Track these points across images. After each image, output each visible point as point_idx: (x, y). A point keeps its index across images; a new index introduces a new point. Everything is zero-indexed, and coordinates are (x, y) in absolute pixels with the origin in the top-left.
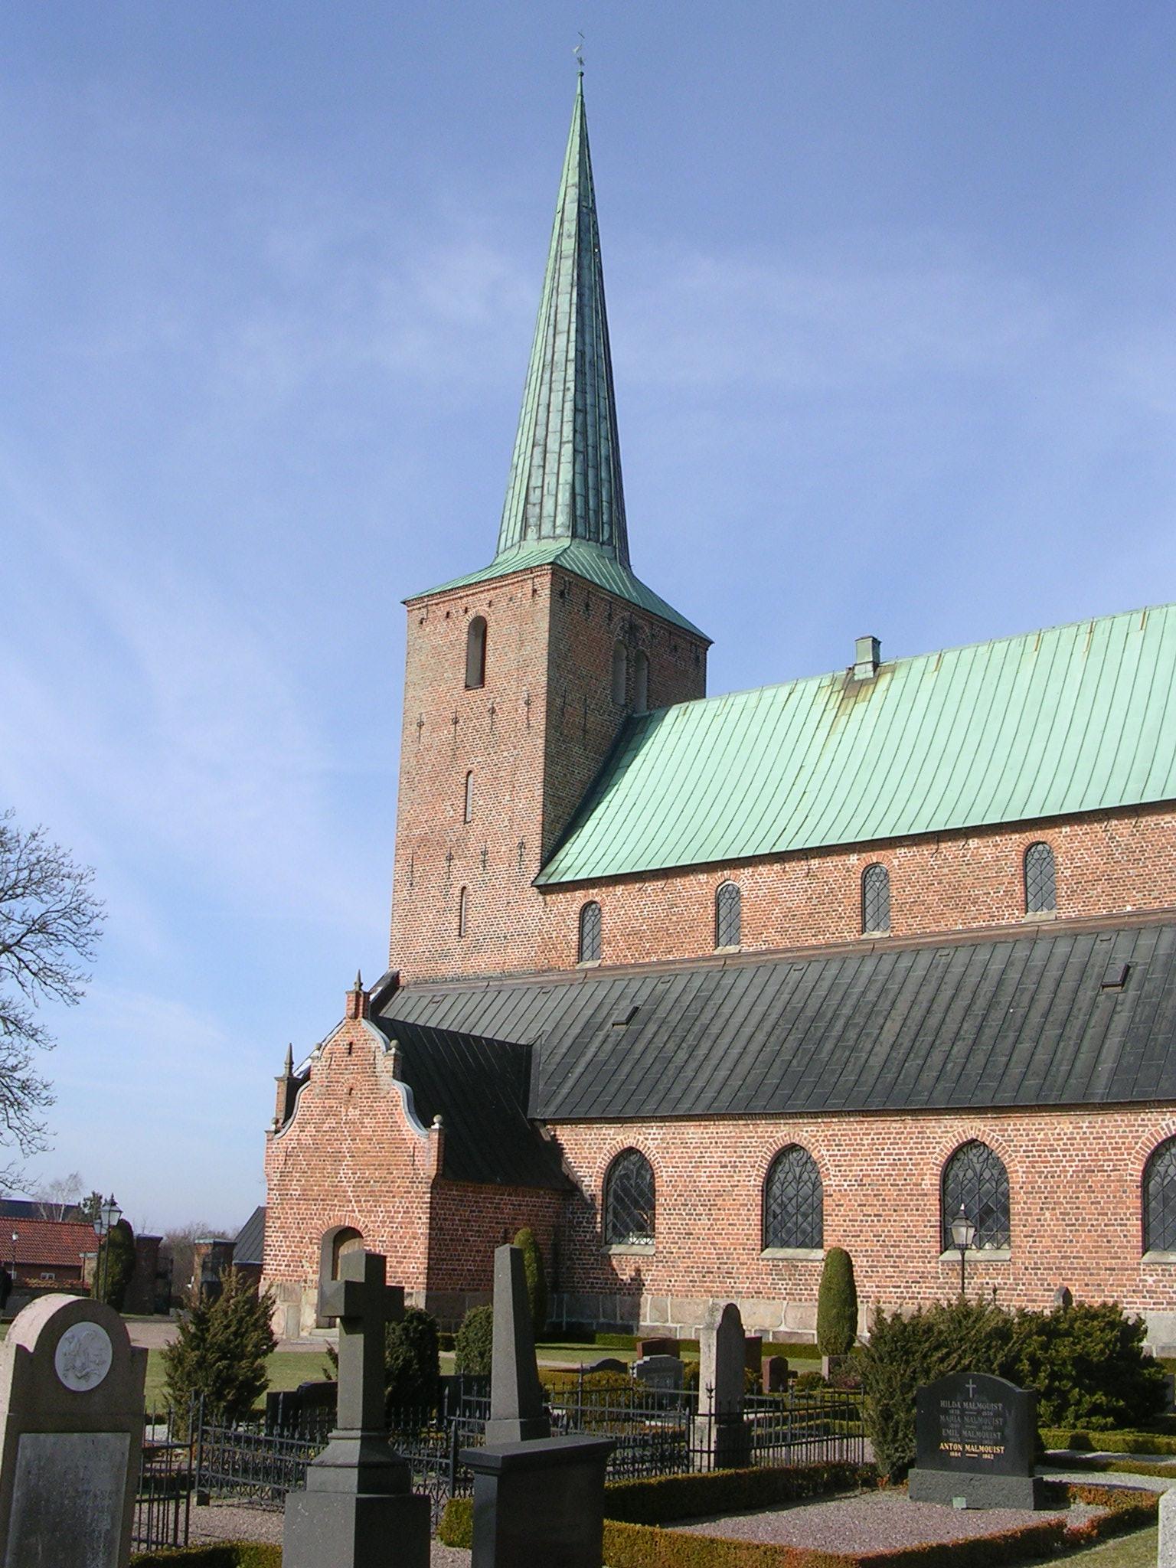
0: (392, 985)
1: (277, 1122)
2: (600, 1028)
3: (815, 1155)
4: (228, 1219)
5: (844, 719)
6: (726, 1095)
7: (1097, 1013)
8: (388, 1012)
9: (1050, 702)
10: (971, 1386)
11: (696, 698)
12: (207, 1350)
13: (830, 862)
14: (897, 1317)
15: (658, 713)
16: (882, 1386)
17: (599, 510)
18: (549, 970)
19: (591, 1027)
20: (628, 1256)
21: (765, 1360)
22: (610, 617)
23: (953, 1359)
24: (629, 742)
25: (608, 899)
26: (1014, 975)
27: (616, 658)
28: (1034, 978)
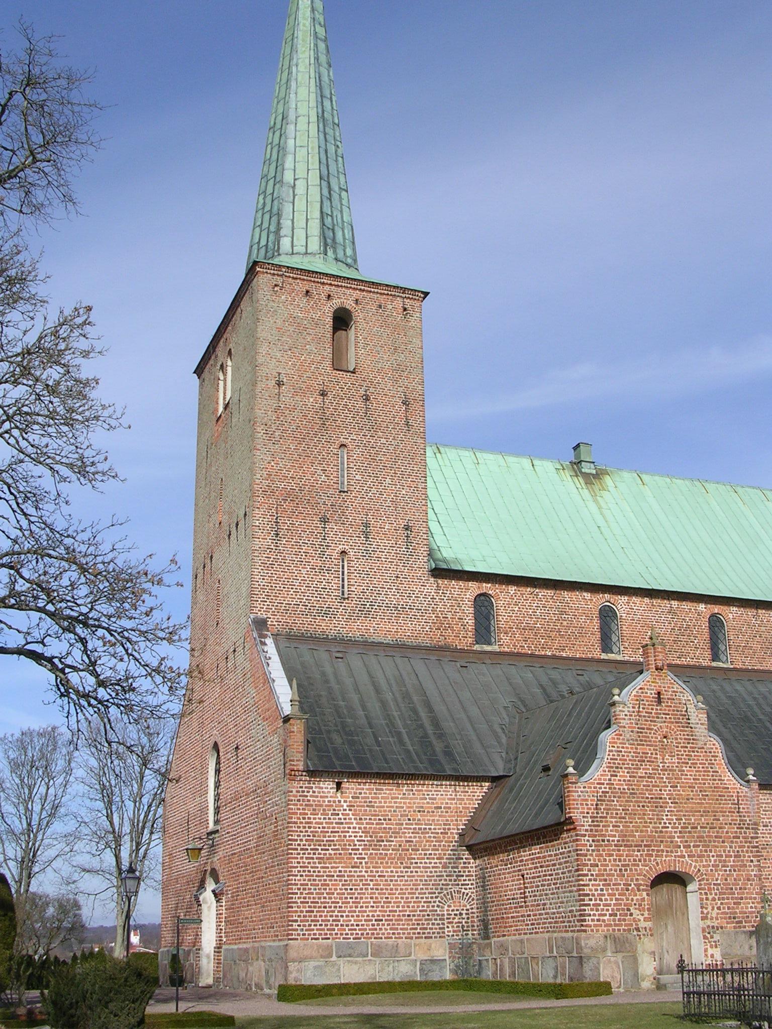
13: (686, 605)
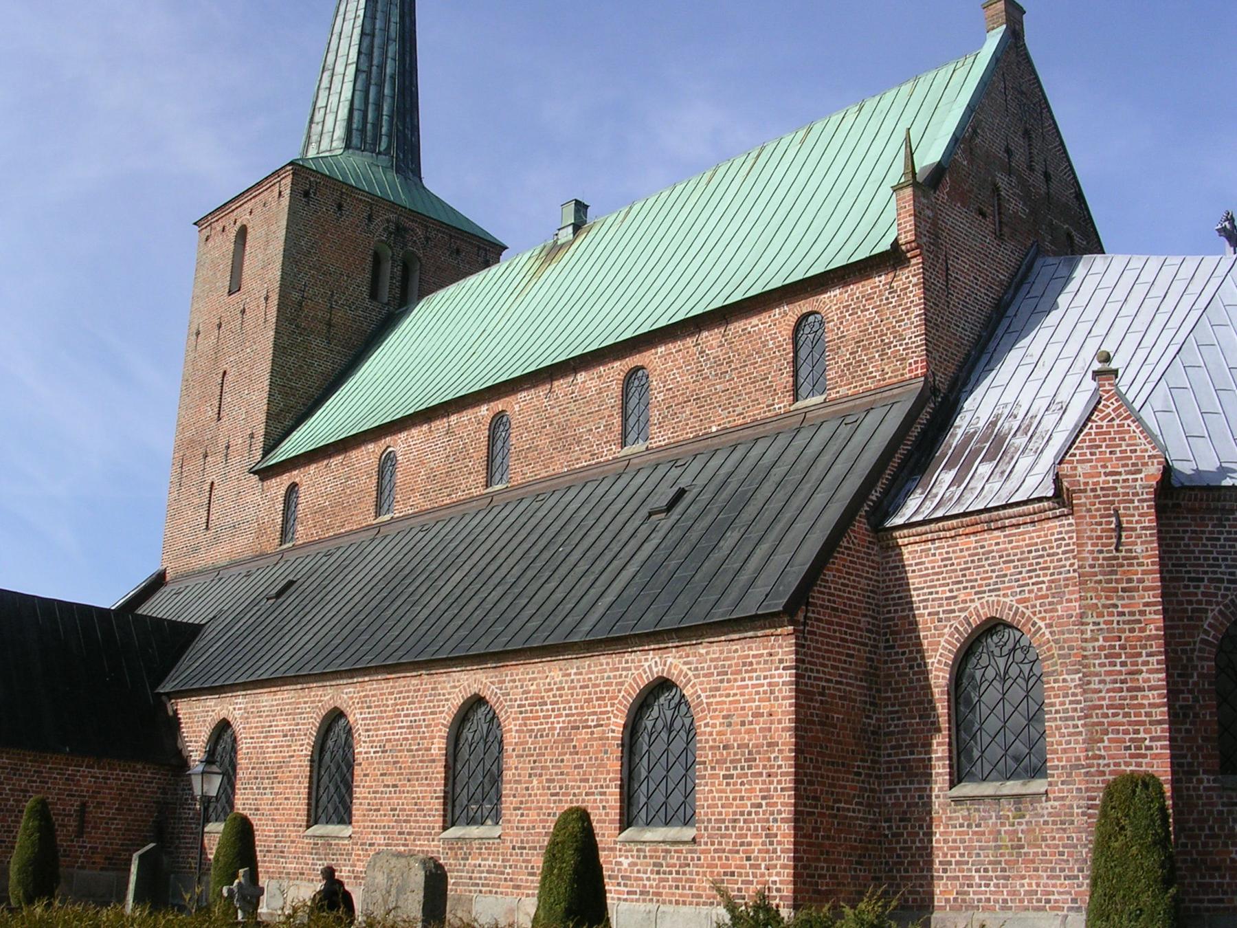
22: (370, 218)
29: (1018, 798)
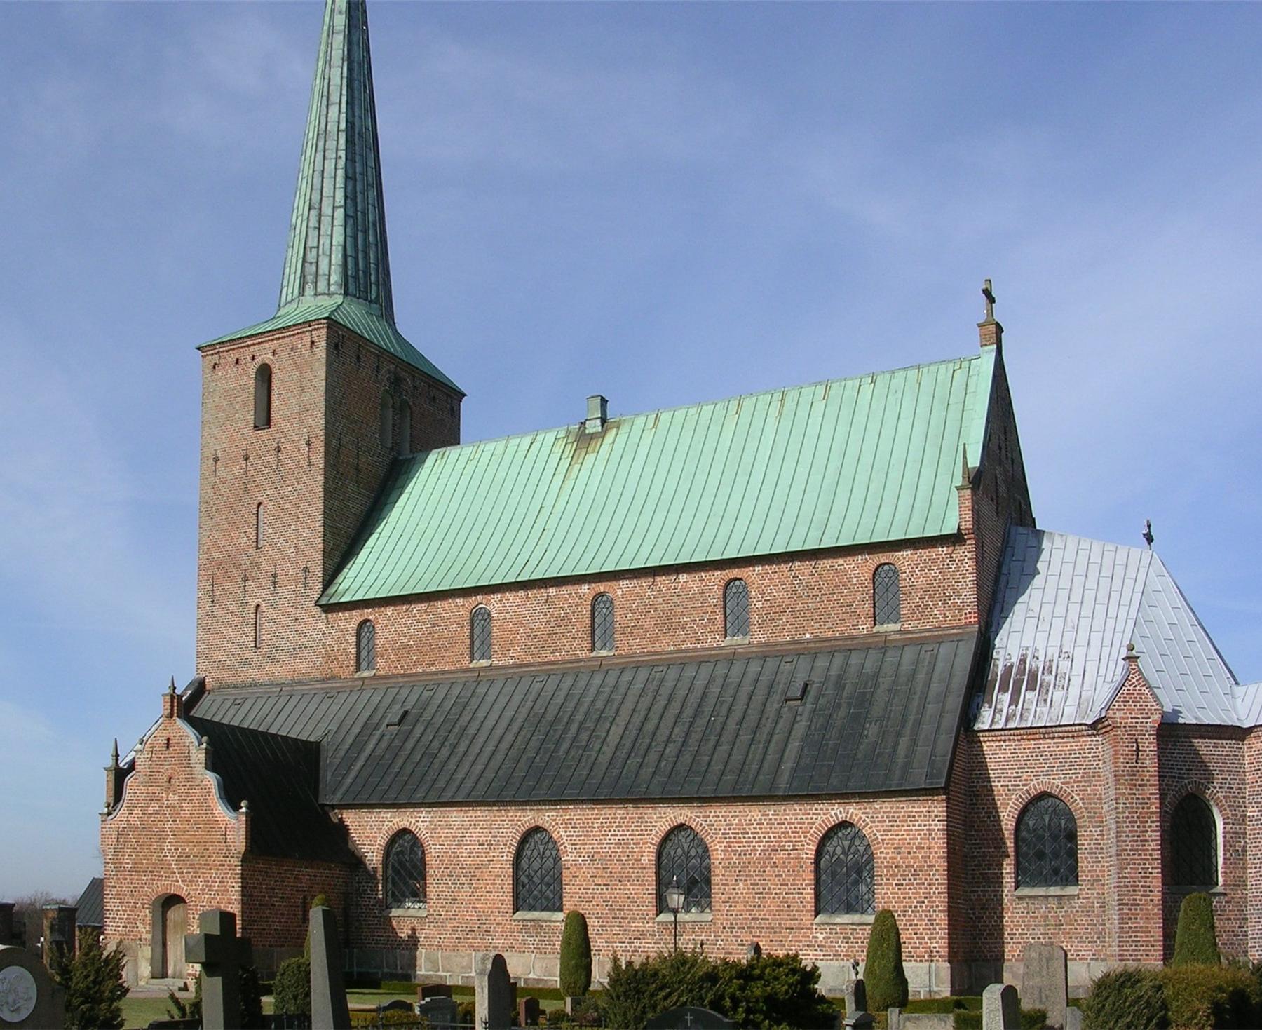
0: (200, 689)
1: (108, 806)
2: (376, 728)
3: (555, 836)
4: (67, 888)
5: (577, 467)
6: (482, 787)
7: (781, 722)
8: (197, 712)
9: (748, 459)
10: (689, 1017)
11: (452, 444)
12: (72, 996)
13: (566, 591)
14: (630, 964)
15: (420, 456)
16: (619, 1018)
17: (367, 271)
18: (333, 678)
19: (369, 727)
20: (405, 917)
21: (521, 1002)
22: (378, 369)
23: (674, 997)
24: (396, 480)
25: (382, 618)
26: (715, 689)
27: (384, 406)
28: (731, 691)
29: (1060, 897)
